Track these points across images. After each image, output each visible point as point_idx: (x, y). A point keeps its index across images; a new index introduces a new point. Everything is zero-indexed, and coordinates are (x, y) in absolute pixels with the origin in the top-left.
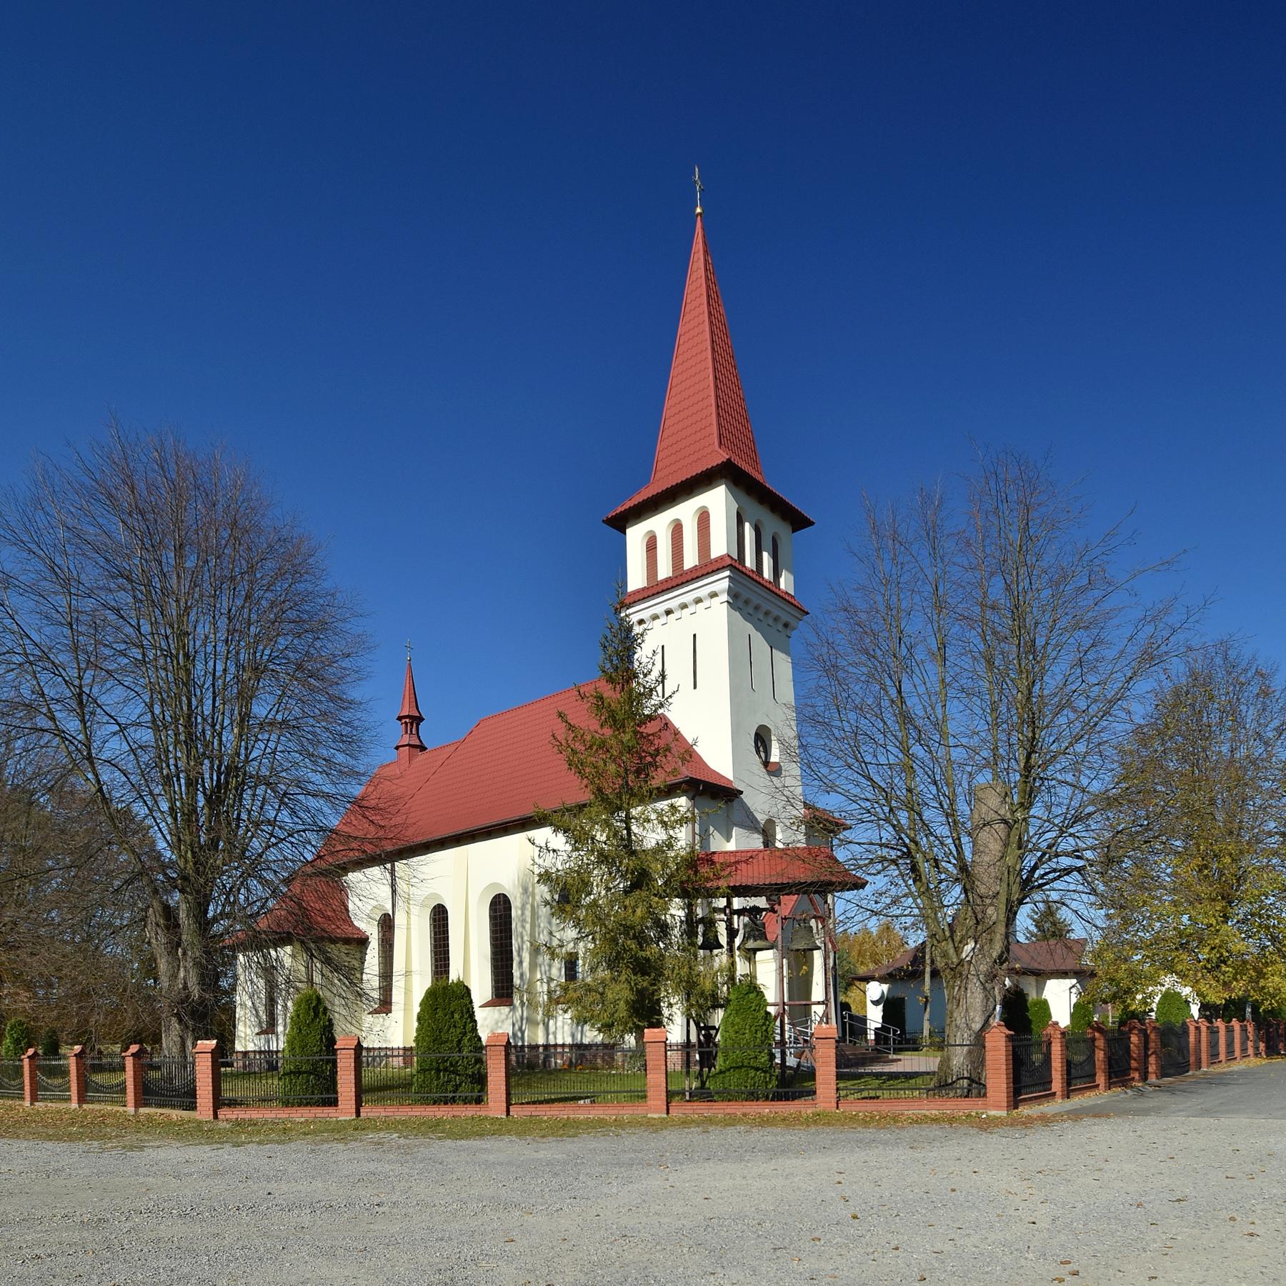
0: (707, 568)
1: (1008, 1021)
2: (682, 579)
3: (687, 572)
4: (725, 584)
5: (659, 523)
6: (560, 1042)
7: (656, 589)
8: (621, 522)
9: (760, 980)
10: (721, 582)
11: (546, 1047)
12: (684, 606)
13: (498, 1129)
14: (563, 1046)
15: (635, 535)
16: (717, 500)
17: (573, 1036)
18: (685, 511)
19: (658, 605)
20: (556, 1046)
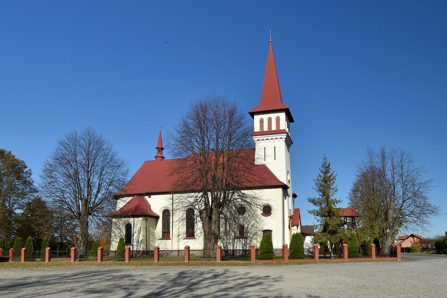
0: (279, 132)
1: (202, 275)
2: (270, 132)
3: (264, 132)
4: (285, 137)
5: (265, 117)
6: (238, 248)
7: (262, 133)
8: (252, 114)
9: (432, 219)
10: (284, 136)
11: (233, 250)
12: (272, 139)
13: (287, 264)
14: (239, 250)
15: (257, 118)
16: (282, 116)
17: (243, 248)
18: (273, 116)
19: (260, 138)
20: (237, 250)
